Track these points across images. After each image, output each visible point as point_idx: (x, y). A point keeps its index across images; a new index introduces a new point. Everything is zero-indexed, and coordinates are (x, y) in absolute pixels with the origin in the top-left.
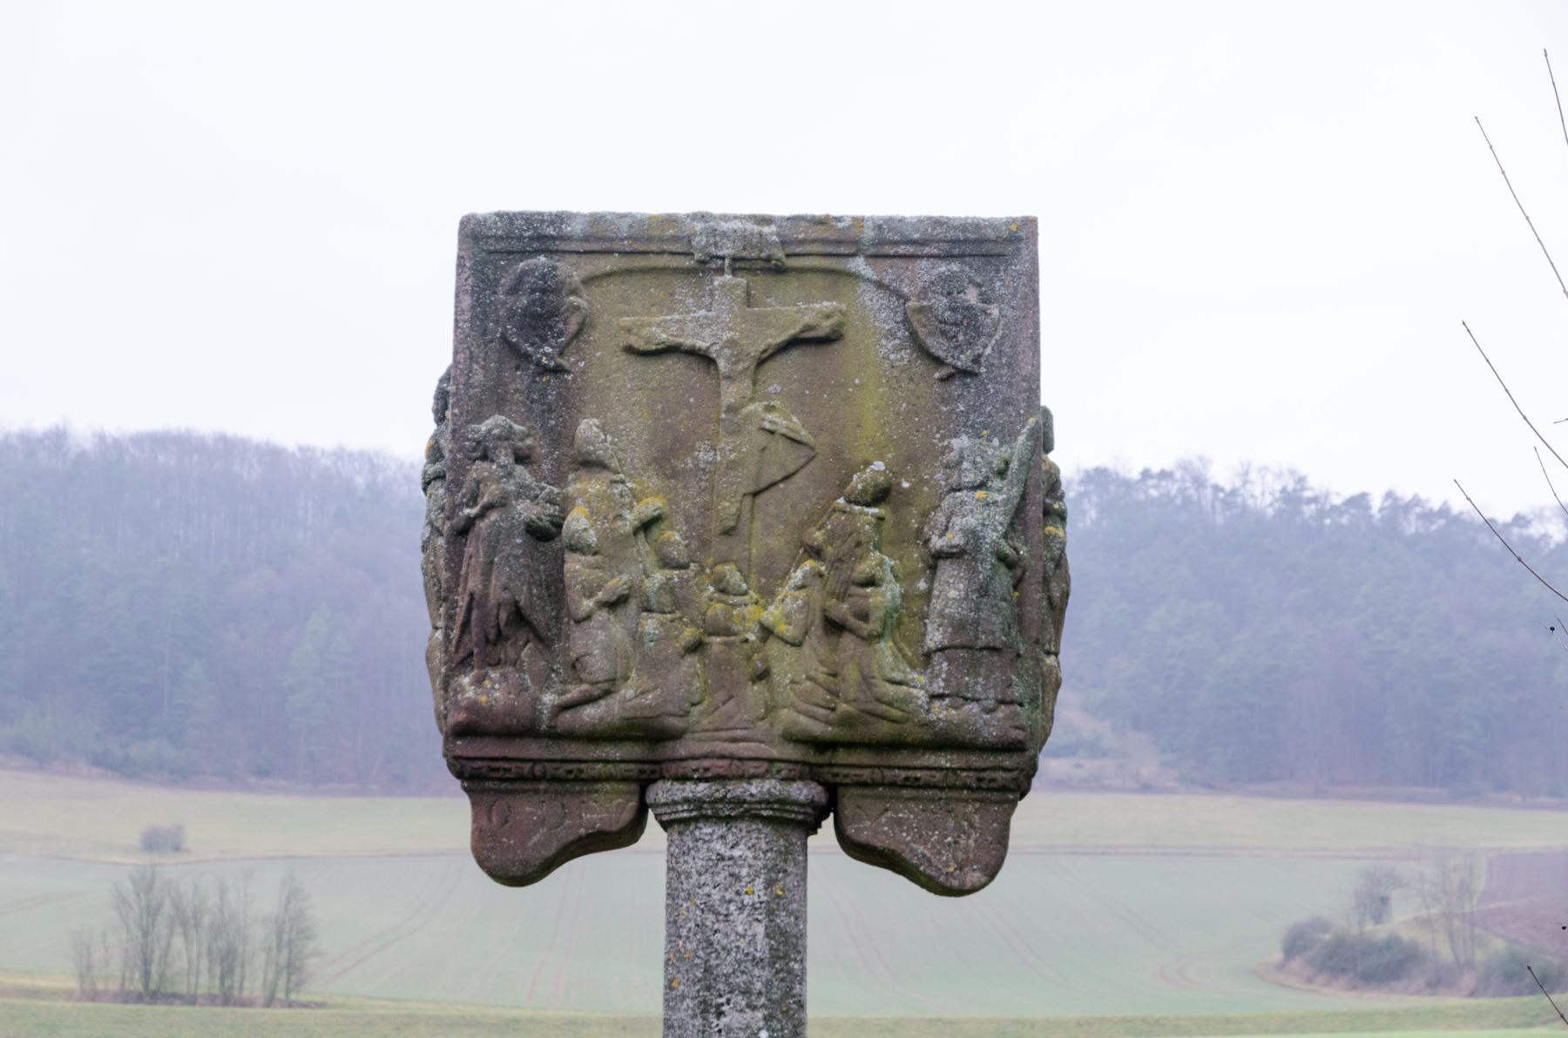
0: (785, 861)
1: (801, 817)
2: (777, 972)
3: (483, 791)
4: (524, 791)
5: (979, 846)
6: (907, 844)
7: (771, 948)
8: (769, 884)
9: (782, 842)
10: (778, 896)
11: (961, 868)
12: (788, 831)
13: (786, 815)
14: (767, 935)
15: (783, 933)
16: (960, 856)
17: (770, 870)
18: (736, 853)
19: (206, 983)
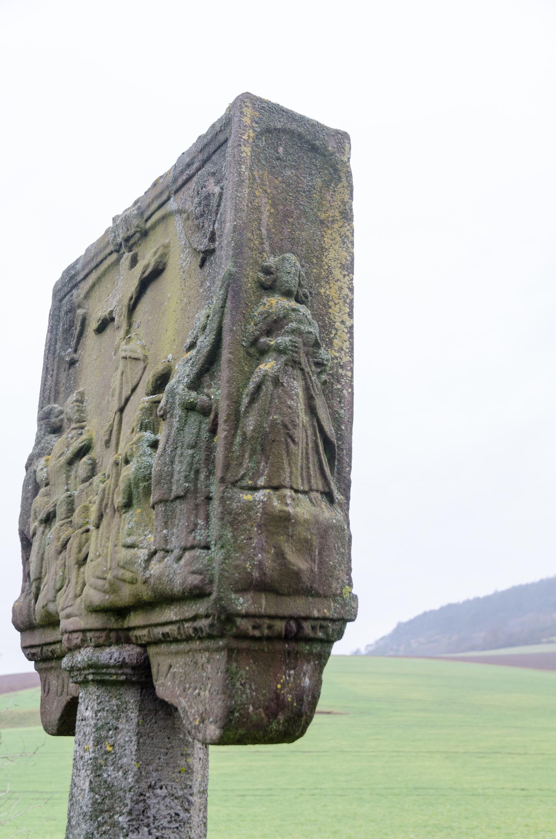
0: (117, 719)
1: (123, 678)
2: (100, 825)
3: (47, 670)
4: (52, 668)
7: (95, 802)
8: (98, 742)
9: (114, 702)
11: (203, 721)
12: (122, 690)
13: (107, 677)
14: (92, 790)
17: (98, 729)
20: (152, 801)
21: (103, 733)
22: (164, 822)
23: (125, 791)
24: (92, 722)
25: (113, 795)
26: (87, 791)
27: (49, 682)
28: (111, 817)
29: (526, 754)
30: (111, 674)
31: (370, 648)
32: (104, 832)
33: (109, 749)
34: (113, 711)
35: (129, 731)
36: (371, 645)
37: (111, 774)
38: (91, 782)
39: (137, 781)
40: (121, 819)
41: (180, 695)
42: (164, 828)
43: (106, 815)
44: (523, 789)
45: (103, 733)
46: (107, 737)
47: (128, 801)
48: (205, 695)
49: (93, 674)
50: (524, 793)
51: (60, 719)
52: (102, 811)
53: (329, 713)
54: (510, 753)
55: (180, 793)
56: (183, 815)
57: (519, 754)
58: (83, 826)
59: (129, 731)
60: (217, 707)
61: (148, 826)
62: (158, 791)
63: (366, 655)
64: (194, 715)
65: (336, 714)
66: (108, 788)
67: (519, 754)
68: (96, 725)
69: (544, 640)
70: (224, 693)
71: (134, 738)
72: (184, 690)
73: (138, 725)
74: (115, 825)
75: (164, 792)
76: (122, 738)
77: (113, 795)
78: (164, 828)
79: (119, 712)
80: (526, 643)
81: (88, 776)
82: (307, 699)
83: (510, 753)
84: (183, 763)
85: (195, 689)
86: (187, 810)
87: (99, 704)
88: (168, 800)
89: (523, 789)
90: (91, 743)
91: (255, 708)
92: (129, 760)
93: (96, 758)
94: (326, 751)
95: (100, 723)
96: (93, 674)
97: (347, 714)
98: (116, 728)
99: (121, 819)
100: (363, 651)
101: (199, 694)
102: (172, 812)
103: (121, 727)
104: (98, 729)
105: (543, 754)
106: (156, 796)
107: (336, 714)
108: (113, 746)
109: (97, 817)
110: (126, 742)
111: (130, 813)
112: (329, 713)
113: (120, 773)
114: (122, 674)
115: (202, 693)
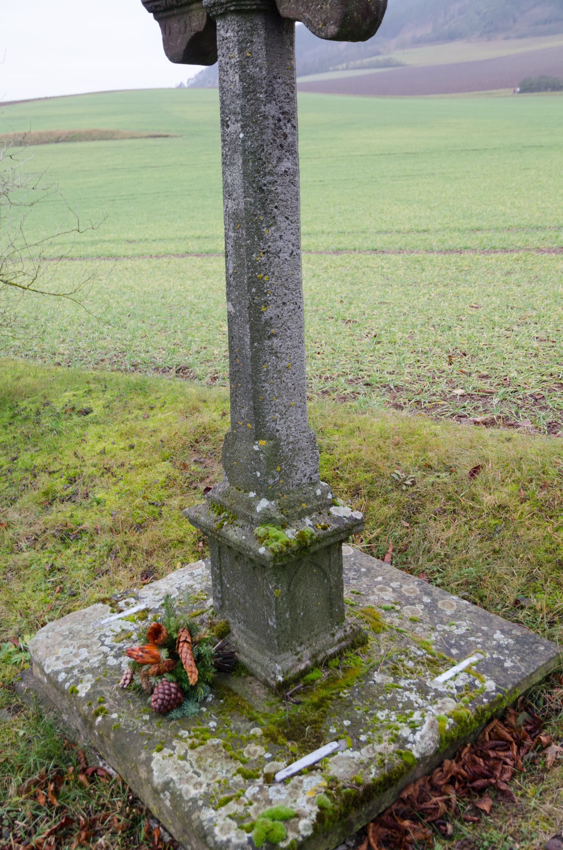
0: (252, 35)
1: (254, 7)
2: (249, 100)
3: (167, 18)
4: (172, 16)
5: (332, 9)
6: (302, 14)
7: (244, 88)
8: (241, 51)
9: (248, 24)
10: (248, 57)
11: (325, 24)
12: (253, 17)
13: (244, 7)
14: (241, 80)
15: (252, 78)
16: (324, 16)
17: (240, 43)
18: (228, 35)
19: (546, 338)
20: (276, 86)
21: (244, 45)
22: (282, 98)
23: (261, 80)
24: (235, 39)
25: (254, 82)
26: (237, 82)
27: (170, 28)
28: (255, 95)
29: (320, 158)
30: (247, 5)
31: (193, 82)
32: (252, 104)
33: (248, 55)
34: (248, 31)
35: (260, 43)
36: (192, 79)
37: (251, 70)
38: (240, 76)
39: (268, 74)
40: (261, 96)
41: (304, 12)
42: (283, 102)
43: (252, 94)
44: (320, 181)
45: (244, 45)
46: (246, 48)
47: (264, 85)
48: (326, 8)
49: (234, 5)
50: (322, 183)
51: (185, 51)
52: (249, 92)
53: (166, 136)
54: (309, 158)
55: (289, 82)
56: (291, 95)
57: (315, 158)
58: (238, 102)
59: (260, 43)
60: (337, 14)
61: (275, 100)
62: (278, 80)
63: (189, 88)
64: (318, 22)
65: (172, 137)
66: (251, 79)
67: (315, 158)
68: (238, 40)
69: (331, 68)
70: (342, 4)
71: (264, 47)
72: (308, 7)
73: (265, 39)
74: (258, 99)
75: (280, 81)
76: (256, 47)
77: (254, 82)
78: (283, 102)
79: (252, 31)
80: (317, 71)
81: (237, 73)
82: (381, 9)
83: (309, 158)
84: (289, 64)
85: (317, 5)
86: (292, 92)
87: (238, 26)
88: (283, 86)
89: (320, 181)
90: (236, 52)
91: (358, 14)
92: (261, 60)
93: (241, 61)
94: (169, 166)
95: (241, 39)
96: (234, 5)
97: (180, 136)
98: (252, 42)
99: (261, 96)
100: (186, 85)
101: (321, 8)
102: (286, 93)
103: (254, 40)
104: (240, 43)
105: (332, 157)
106: (278, 83)
107: (172, 137)
108: (250, 53)
109: (246, 96)
110: (259, 50)
111: (266, 92)
112: (166, 136)
113: (258, 69)
114: (254, 5)
115: (324, 7)
